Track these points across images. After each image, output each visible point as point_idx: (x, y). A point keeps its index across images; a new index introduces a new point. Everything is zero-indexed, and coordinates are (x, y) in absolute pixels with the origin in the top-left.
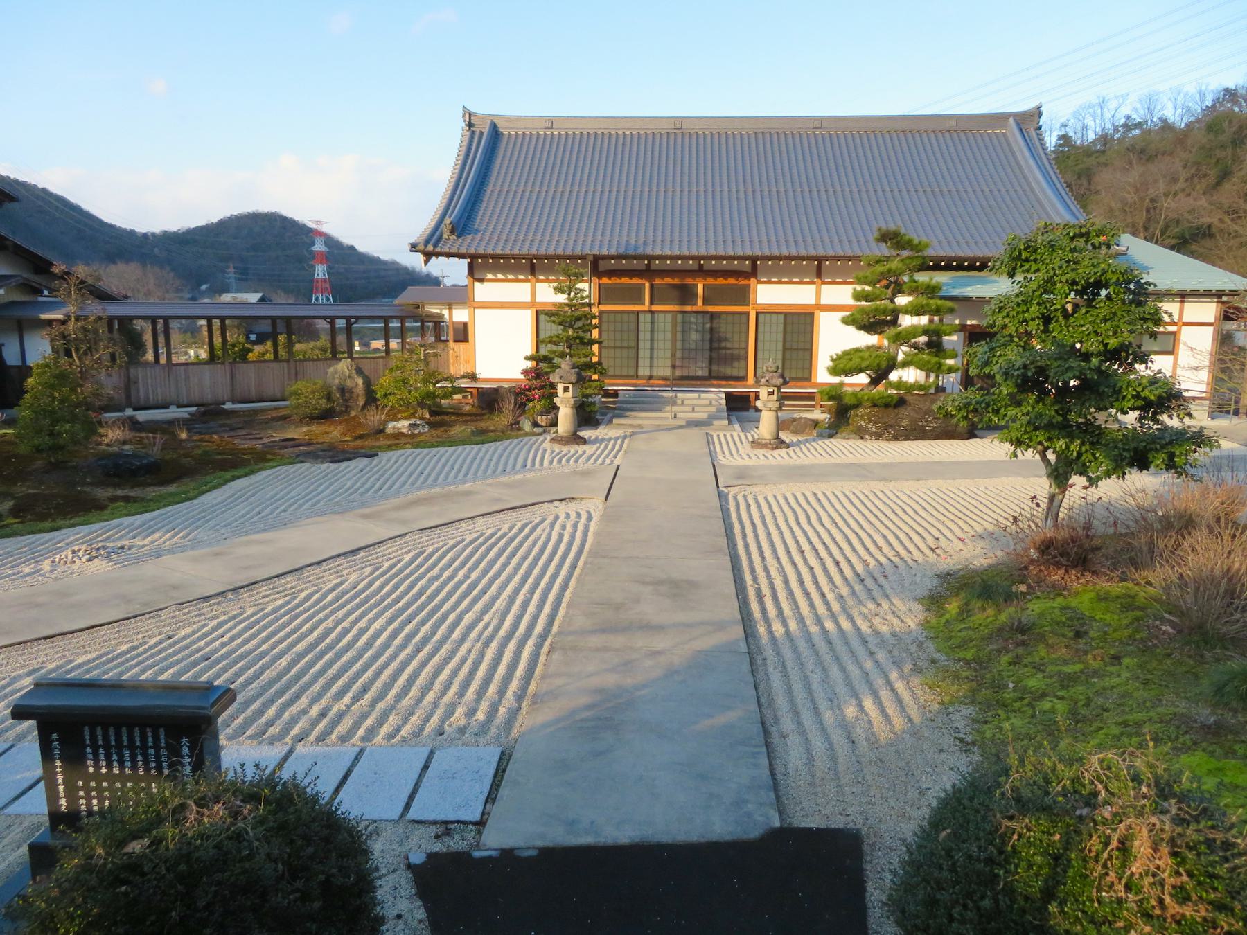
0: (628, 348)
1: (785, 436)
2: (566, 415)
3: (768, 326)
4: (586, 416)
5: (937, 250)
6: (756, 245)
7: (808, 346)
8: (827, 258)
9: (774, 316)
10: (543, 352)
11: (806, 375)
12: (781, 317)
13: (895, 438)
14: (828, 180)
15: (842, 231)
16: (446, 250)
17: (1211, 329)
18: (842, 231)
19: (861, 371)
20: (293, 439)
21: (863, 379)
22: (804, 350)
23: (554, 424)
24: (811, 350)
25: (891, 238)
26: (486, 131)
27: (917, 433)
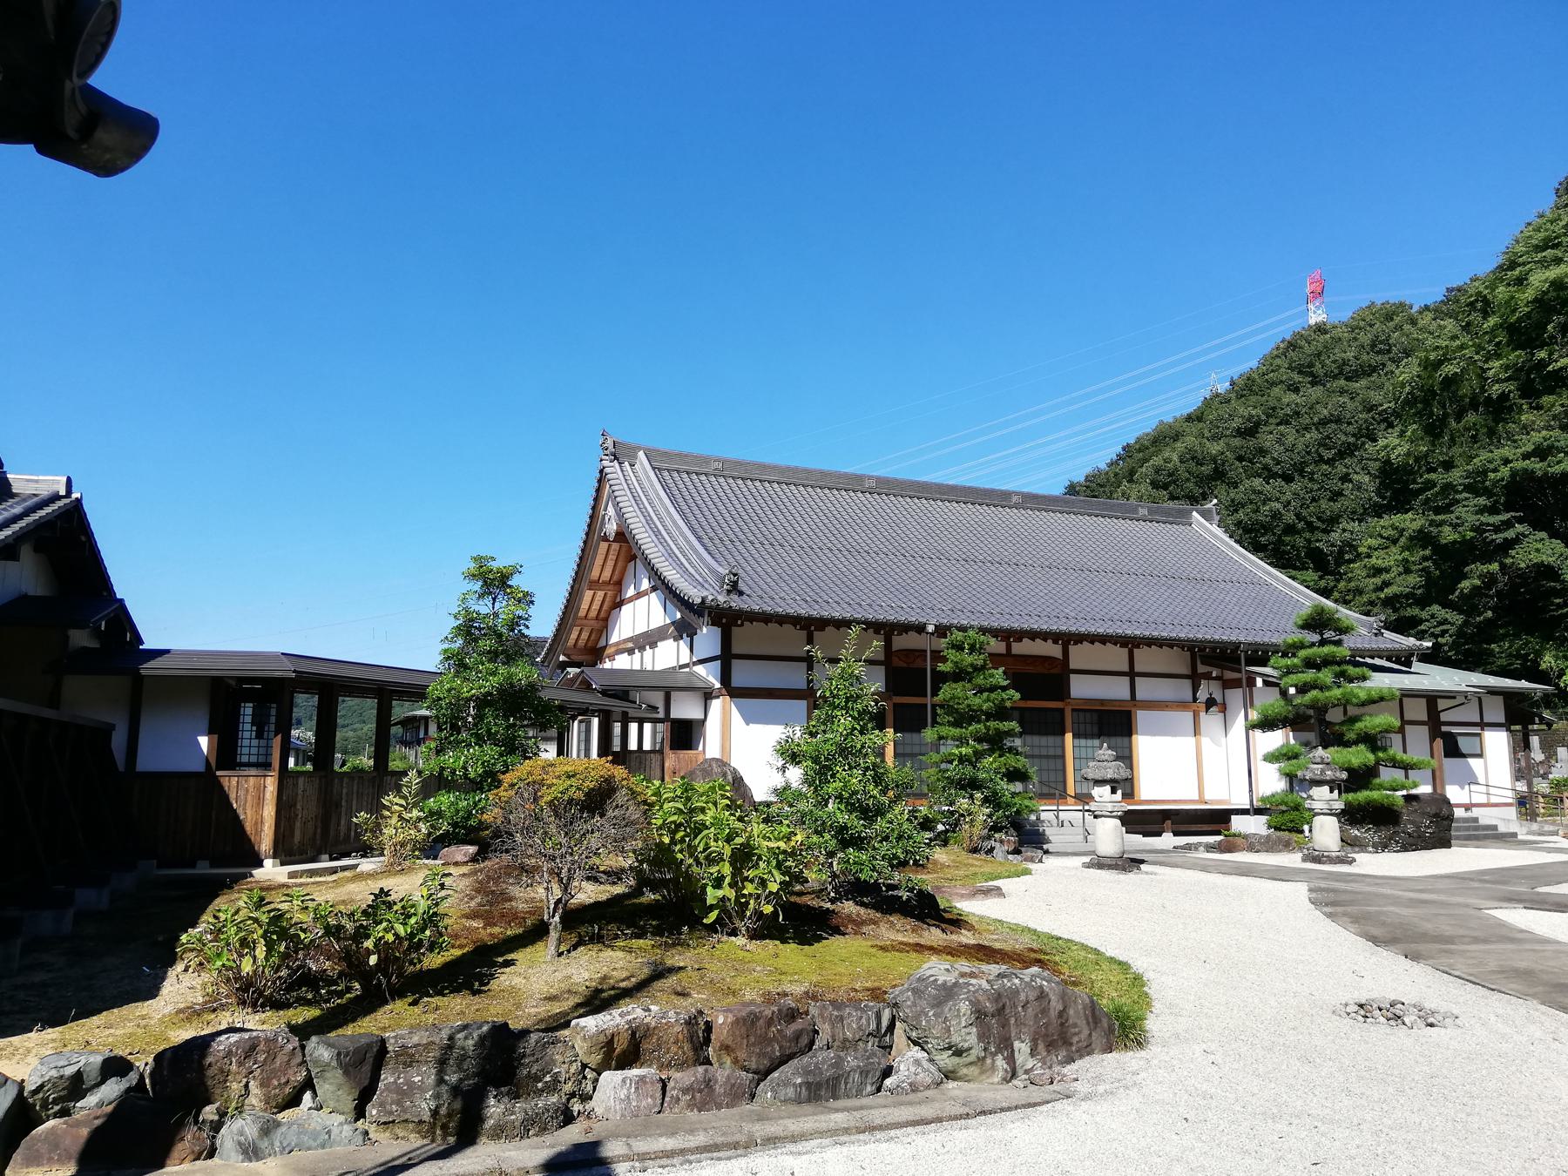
13: (1405, 849)
22: (1055, 757)
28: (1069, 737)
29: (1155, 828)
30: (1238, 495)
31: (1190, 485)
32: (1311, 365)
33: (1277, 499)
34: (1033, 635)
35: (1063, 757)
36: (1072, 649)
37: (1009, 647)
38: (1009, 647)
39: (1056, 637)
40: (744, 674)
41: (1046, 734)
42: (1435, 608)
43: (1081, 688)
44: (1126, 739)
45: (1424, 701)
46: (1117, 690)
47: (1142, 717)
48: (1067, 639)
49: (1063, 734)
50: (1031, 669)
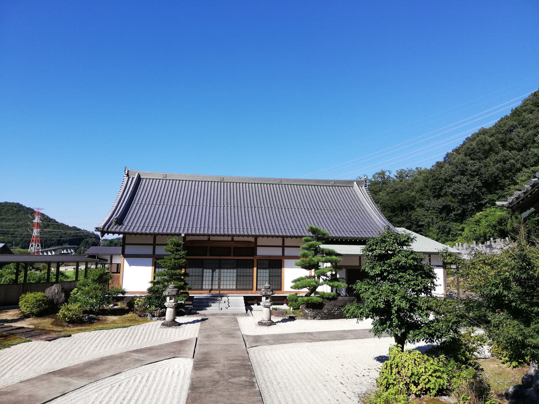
0: (198, 276)
1: (274, 319)
2: (170, 311)
3: (262, 278)
4: (179, 311)
5: (332, 234)
6: (257, 230)
7: (279, 275)
8: (287, 237)
10: (157, 279)
12: (267, 261)
13: (322, 318)
14: (288, 204)
16: (113, 230)
19: (304, 287)
20: (23, 328)
21: (306, 290)
22: (278, 276)
23: (164, 314)
24: (281, 276)
25: (314, 231)
28: (255, 269)
29: (281, 302)
30: (498, 157)
31: (480, 154)
33: (514, 159)
35: (253, 276)
41: (247, 268)
42: (459, 212)
43: (261, 252)
44: (280, 270)
46: (278, 252)
47: (286, 262)
48: (256, 237)
49: (253, 268)
50: (241, 246)
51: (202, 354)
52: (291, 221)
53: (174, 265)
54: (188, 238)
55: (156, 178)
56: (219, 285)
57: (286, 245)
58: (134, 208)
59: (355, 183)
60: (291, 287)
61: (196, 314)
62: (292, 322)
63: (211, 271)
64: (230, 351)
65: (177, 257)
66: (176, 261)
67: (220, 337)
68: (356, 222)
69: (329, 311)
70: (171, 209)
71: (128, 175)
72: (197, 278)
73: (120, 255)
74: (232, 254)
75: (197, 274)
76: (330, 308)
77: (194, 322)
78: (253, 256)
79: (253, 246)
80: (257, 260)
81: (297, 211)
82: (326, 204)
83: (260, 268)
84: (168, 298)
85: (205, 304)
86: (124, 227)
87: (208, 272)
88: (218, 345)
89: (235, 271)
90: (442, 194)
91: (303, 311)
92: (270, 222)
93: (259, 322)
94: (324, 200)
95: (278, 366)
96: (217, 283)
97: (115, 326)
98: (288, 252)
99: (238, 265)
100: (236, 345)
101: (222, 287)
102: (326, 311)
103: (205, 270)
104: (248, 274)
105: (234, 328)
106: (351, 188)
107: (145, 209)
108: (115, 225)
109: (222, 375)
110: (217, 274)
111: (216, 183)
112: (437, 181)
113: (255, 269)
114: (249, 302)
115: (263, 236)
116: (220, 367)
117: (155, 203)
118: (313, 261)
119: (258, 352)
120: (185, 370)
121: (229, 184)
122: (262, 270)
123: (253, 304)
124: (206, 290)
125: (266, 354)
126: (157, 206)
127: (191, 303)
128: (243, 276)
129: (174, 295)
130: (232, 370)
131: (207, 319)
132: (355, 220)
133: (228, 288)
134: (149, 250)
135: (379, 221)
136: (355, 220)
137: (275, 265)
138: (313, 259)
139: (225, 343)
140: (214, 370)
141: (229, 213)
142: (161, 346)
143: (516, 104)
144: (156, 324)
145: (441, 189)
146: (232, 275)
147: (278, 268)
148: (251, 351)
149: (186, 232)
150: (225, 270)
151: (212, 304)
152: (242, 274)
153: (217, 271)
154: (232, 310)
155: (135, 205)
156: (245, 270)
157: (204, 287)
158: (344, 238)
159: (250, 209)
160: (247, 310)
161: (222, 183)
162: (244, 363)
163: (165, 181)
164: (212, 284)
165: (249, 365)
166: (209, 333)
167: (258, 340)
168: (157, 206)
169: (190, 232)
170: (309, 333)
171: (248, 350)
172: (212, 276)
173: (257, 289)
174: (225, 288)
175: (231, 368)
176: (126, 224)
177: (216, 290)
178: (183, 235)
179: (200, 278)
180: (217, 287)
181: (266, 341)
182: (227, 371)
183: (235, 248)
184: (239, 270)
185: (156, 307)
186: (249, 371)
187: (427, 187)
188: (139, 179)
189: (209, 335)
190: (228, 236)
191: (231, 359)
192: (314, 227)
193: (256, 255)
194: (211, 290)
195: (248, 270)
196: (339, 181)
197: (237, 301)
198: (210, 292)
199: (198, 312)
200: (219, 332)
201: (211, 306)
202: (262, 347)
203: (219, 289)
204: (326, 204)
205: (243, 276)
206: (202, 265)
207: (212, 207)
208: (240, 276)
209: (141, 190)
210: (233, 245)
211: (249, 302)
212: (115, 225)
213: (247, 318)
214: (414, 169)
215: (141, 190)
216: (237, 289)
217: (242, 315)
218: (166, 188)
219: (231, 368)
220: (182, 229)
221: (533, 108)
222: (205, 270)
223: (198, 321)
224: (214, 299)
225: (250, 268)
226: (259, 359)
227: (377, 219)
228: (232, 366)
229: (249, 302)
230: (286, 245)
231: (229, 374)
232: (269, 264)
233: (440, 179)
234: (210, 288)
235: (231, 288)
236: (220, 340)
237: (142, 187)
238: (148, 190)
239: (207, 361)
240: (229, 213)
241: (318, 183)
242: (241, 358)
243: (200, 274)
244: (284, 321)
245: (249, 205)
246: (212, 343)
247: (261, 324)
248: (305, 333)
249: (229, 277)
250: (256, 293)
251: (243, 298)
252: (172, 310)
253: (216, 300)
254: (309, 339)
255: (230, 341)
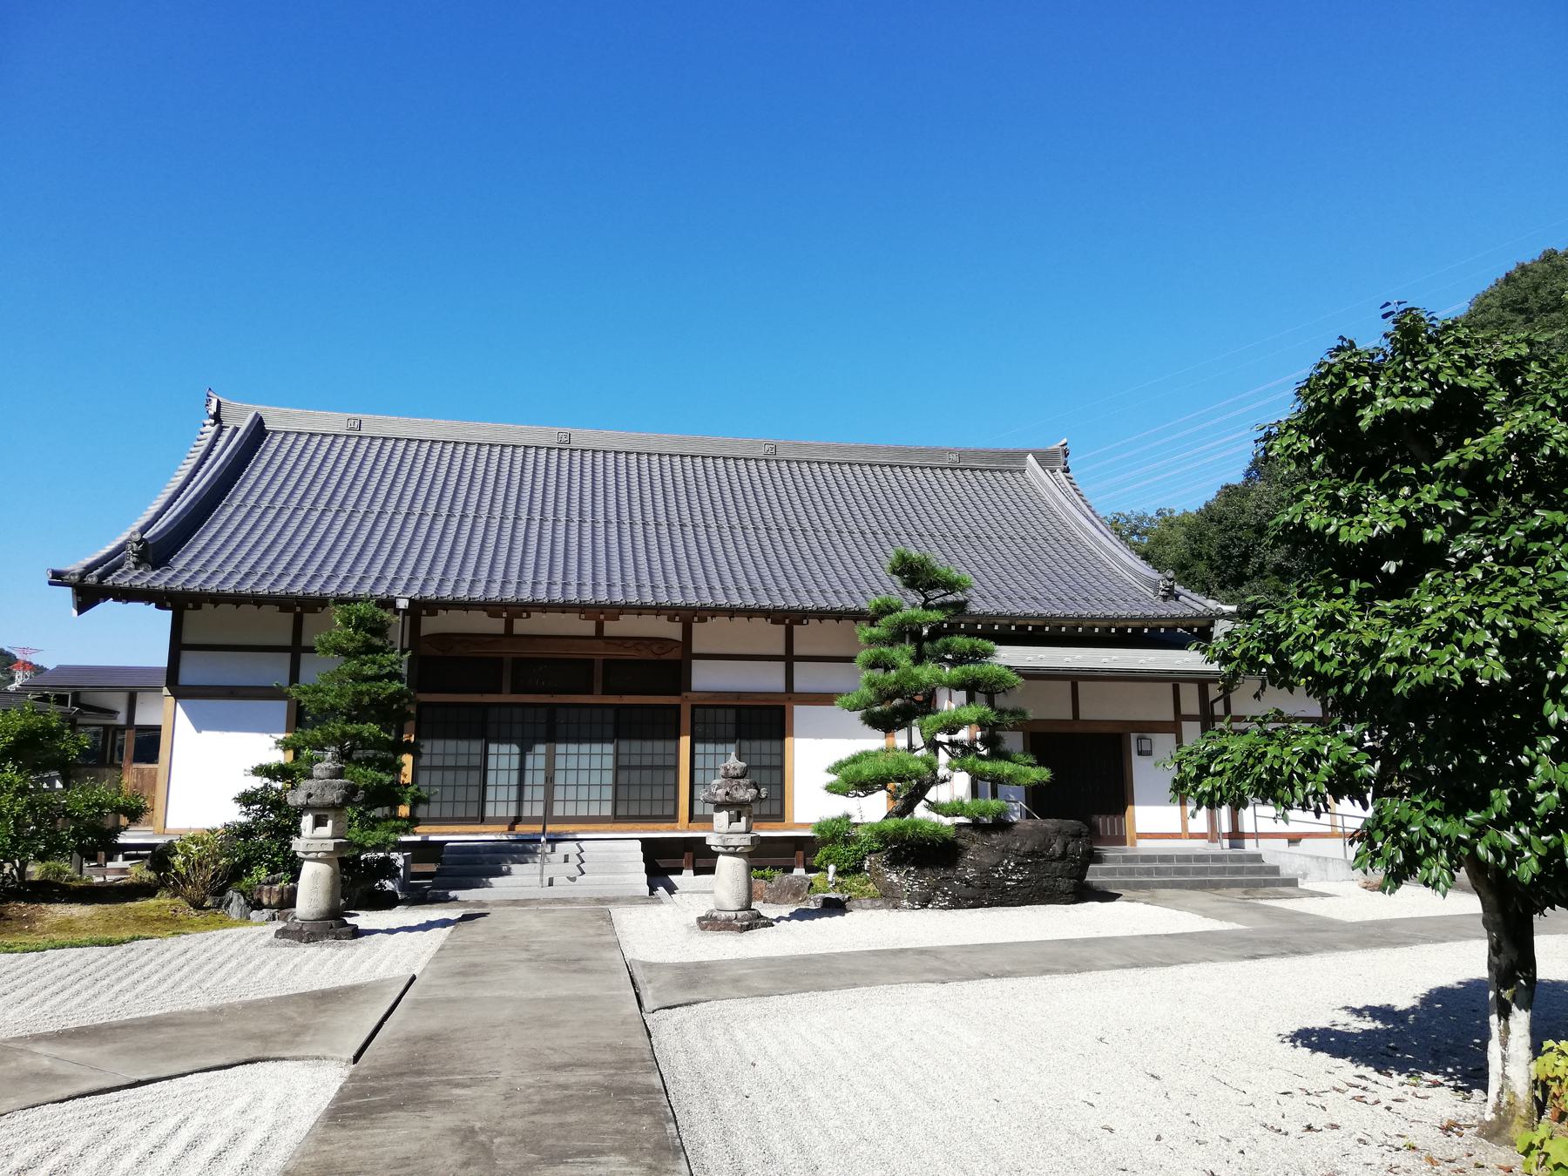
0: (468, 768)
2: (316, 875)
9: (721, 712)
11: (776, 810)
12: (731, 714)
13: (957, 903)
15: (821, 578)
17: (1068, 715)
18: (821, 578)
22: (664, 767)
24: (781, 768)
26: (244, 426)
27: (990, 893)
28: (685, 741)
32: (1526, 300)
34: (641, 609)
35: (676, 767)
36: (697, 628)
37: (600, 627)
38: (600, 627)
39: (672, 612)
40: (190, 673)
41: (653, 737)
43: (706, 678)
44: (776, 744)
45: (1195, 686)
46: (769, 679)
47: (801, 714)
48: (688, 616)
51: (411, 1040)
52: (815, 567)
53: (357, 705)
54: (430, 625)
55: (324, 430)
56: (549, 802)
57: (798, 651)
58: (223, 518)
59: (1030, 457)
60: (831, 789)
61: (443, 900)
62: (838, 918)
63: (515, 749)
64: (556, 1025)
65: (369, 670)
66: (364, 687)
67: (522, 973)
68: (1048, 571)
69: (985, 872)
70: (368, 525)
71: (217, 417)
72: (462, 776)
73: (158, 689)
74: (598, 686)
75: (463, 762)
76: (987, 859)
77: (428, 926)
78: (677, 692)
79: (675, 655)
80: (693, 707)
81: (835, 538)
82: (937, 519)
83: (704, 740)
84: (307, 821)
85: (487, 866)
86: (170, 574)
87: (503, 757)
88: (502, 1000)
89: (609, 748)
90: (1249, 571)
91: (876, 877)
92: (738, 568)
93: (700, 919)
94: (930, 508)
95: (812, 1092)
96: (540, 793)
97: (69, 938)
98: (808, 677)
99: (621, 727)
100: (594, 998)
101: (558, 811)
102: (970, 873)
103: (493, 748)
104: (658, 761)
105: (596, 939)
106: (1018, 475)
107: (265, 524)
108: (137, 565)
109: (486, 1149)
110: (541, 762)
111: (543, 452)
112: (1232, 533)
113: (685, 741)
114: (664, 861)
115: (716, 611)
116: (481, 1105)
117: (307, 504)
118: (915, 678)
119: (702, 1026)
120: (275, 1127)
121: (589, 455)
122: (710, 748)
123: (679, 871)
124: (496, 821)
125: (740, 1035)
126: (315, 515)
127: (432, 868)
128: (641, 767)
129: (332, 807)
130: (549, 1119)
131: (484, 915)
132: (1044, 568)
133: (583, 812)
134: (274, 670)
135: (1130, 569)
136: (1044, 568)
137: (761, 724)
138: (916, 670)
139: (542, 994)
140: (441, 1121)
141: (587, 542)
142: (216, 1011)
143: (1456, 307)
144: (262, 929)
145: (1245, 557)
146: (596, 763)
147: (770, 737)
148: (666, 1026)
149: (414, 592)
150: (573, 748)
151: (515, 868)
152: (635, 761)
153: (540, 748)
154: (592, 883)
155: (230, 510)
156: (648, 746)
157: (489, 812)
158: (1013, 618)
159: (664, 530)
160: (652, 890)
161: (566, 454)
162: (626, 1079)
163: (353, 441)
164: (520, 801)
165: (650, 1090)
166: (477, 960)
167: (695, 982)
168: (315, 515)
169: (430, 593)
170: (922, 952)
171: (649, 1019)
172: (522, 770)
173: (691, 818)
174: (570, 812)
175: (546, 1107)
176: (179, 566)
177: (533, 820)
178: (403, 604)
179: (475, 777)
180: (539, 811)
181: (736, 981)
182: (518, 1124)
183: (609, 664)
184: (625, 746)
185: (273, 869)
186: (646, 1121)
187: (1199, 556)
188: (258, 432)
189: (475, 965)
190: (582, 609)
191: (557, 1059)
192: (915, 553)
193: (689, 689)
194: (518, 820)
195: (659, 746)
196: (976, 454)
197: (619, 856)
198: (511, 829)
199: (452, 894)
200: (525, 955)
201: (508, 873)
202: (717, 1005)
203: (548, 818)
204: (937, 519)
205: (641, 767)
206: (483, 727)
207: (522, 524)
208: (629, 768)
209: (261, 465)
210: (600, 652)
211: (663, 863)
212: (137, 565)
213: (653, 910)
214: (1152, 514)
215: (261, 465)
216: (616, 818)
217: (633, 900)
218: (357, 462)
219: (546, 1107)
220: (401, 584)
221: (1508, 315)
222: (493, 748)
223: (444, 923)
224: (522, 850)
225: (664, 737)
226: (707, 1056)
227: (1123, 564)
228: (552, 1095)
229: (664, 861)
230: (798, 651)
231: (530, 1141)
232: (738, 722)
233: (1240, 528)
234: (513, 813)
235: (594, 812)
236: (524, 984)
237: (267, 457)
238: (288, 467)
239: (420, 1073)
240: (587, 542)
241: (902, 461)
242: (608, 1057)
243: (476, 761)
244: (801, 915)
245: (662, 519)
246: (480, 993)
247: (709, 923)
248: (902, 951)
249: (586, 768)
250: (689, 829)
251: (639, 844)
252: (324, 870)
253: (534, 853)
254: (931, 970)
255: (566, 986)
